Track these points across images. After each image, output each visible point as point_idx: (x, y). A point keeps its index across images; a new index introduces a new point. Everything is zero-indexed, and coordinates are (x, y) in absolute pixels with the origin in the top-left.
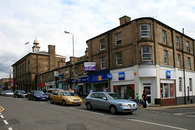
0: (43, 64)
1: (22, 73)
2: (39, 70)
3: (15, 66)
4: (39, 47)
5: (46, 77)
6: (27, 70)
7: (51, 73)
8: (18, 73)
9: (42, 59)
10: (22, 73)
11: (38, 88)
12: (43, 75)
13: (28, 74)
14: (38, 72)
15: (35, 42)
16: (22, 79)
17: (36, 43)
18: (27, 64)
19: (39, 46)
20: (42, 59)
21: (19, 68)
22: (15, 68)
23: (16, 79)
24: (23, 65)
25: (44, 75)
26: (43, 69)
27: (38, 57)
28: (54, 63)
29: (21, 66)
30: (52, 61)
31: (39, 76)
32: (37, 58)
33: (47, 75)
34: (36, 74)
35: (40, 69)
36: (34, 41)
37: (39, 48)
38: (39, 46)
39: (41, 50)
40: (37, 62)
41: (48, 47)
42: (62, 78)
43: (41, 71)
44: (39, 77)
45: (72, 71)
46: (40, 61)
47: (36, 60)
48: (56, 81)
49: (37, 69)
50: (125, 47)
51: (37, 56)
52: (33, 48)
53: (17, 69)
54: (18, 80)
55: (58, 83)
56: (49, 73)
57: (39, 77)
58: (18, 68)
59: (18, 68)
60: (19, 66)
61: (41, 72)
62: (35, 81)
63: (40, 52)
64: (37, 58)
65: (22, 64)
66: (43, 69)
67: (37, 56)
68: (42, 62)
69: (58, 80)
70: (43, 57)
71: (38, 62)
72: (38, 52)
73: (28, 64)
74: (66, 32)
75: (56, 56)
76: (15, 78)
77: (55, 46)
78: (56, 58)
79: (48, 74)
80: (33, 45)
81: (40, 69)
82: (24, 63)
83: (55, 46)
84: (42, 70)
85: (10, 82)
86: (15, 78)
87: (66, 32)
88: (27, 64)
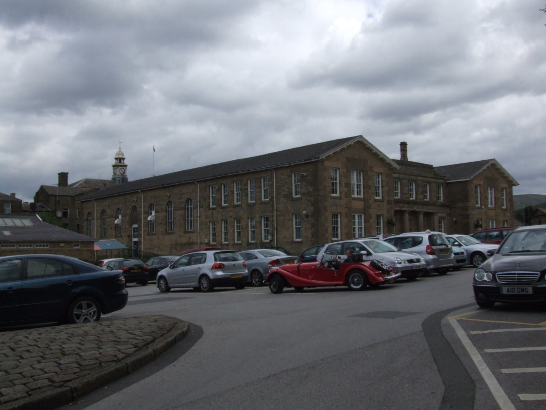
37: (124, 168)
52: (114, 166)
80: (114, 162)
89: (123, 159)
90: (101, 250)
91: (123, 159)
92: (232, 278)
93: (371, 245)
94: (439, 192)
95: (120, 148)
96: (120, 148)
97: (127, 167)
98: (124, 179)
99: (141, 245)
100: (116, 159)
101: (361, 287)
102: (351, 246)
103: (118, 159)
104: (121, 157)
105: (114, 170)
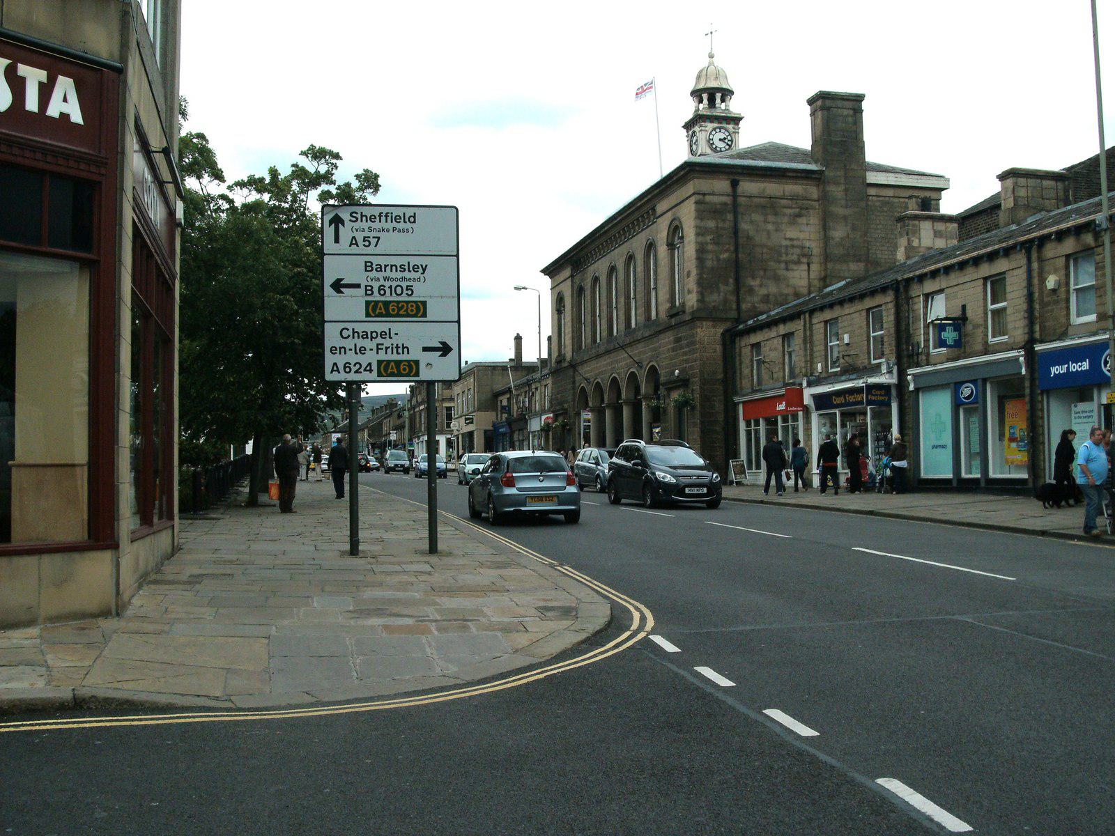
0: (778, 240)
1: (601, 327)
2: (751, 291)
3: (567, 272)
4: (736, 120)
5: (808, 340)
6: (663, 294)
7: (848, 309)
8: (586, 317)
9: (770, 206)
10: (601, 327)
11: (742, 426)
12: (782, 329)
13: (669, 328)
14: (744, 306)
15: (701, 86)
16: (619, 366)
17: (712, 93)
18: (662, 250)
19: (734, 106)
20: (773, 207)
21: (596, 280)
22: (567, 289)
23: (573, 366)
24: (630, 258)
25: (797, 326)
26: (777, 278)
27: (740, 190)
28: (854, 228)
29: (612, 269)
30: (845, 218)
31: (754, 339)
32: (734, 195)
33: (819, 328)
34: (728, 325)
35: (755, 283)
36: (699, 77)
37: (730, 127)
38: (734, 106)
39: (748, 137)
40: (736, 231)
41: (808, 109)
42: (958, 344)
43: (766, 299)
44: (756, 346)
45: (1051, 282)
46: (757, 217)
47: (730, 217)
48: (902, 375)
49: (737, 280)
50: (29, 468)
51: (734, 184)
52: (688, 126)
53: (579, 292)
54: (596, 371)
55: (917, 390)
56: (837, 312)
57: (756, 346)
58: (588, 285)
59: (588, 285)
60: (599, 267)
61: (762, 307)
62: (720, 376)
63: (741, 155)
64: (734, 195)
65: (617, 256)
66: (777, 278)
67: (734, 184)
68: (770, 227)
69: (918, 365)
70: (772, 188)
71: (744, 226)
72: (732, 157)
73: (671, 246)
74: (517, 288)
75: (872, 178)
76: (569, 355)
77: (859, 99)
78: (872, 191)
79: (828, 315)
80: (689, 108)
81: (755, 283)
82: (637, 244)
83: (859, 99)
84: (772, 289)
85: (648, 404)
86: (569, 355)
87: (517, 288)
88: (662, 250)
89: (726, 93)
90: (90, 283)
91: (726, 93)
92: (357, 436)
93: (138, 442)
94: (169, 78)
95: (711, 56)
96: (711, 56)
97: (742, 123)
98: (866, 170)
99: (181, 295)
100: (697, 94)
101: (894, 775)
102: (262, 440)
103: (705, 96)
104: (713, 84)
105: (692, 139)
